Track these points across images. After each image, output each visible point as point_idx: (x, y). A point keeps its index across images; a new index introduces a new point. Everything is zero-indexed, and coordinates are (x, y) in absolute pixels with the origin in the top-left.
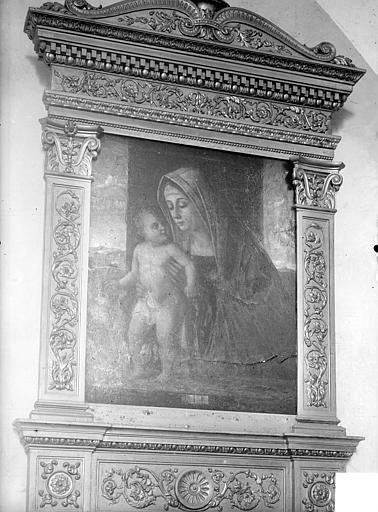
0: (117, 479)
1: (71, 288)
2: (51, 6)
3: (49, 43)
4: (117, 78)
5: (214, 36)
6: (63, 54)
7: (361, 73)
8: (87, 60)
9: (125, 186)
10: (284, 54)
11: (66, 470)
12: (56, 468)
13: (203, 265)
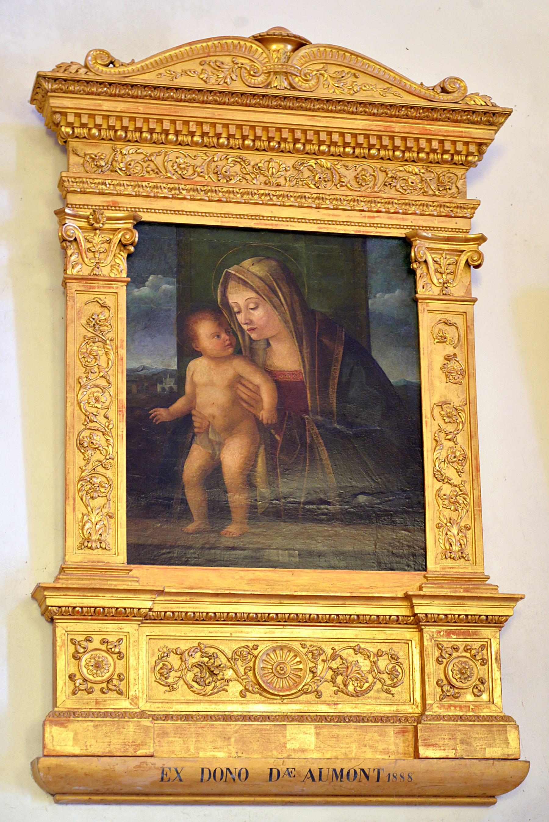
0: (174, 661)
1: (104, 421)
2: (66, 67)
3: (65, 114)
4: (158, 150)
5: (290, 84)
6: (83, 126)
7: (507, 114)
8: (116, 131)
9: (232, 442)
10: (390, 99)
11: (104, 647)
12: (91, 646)
13: (284, 388)
